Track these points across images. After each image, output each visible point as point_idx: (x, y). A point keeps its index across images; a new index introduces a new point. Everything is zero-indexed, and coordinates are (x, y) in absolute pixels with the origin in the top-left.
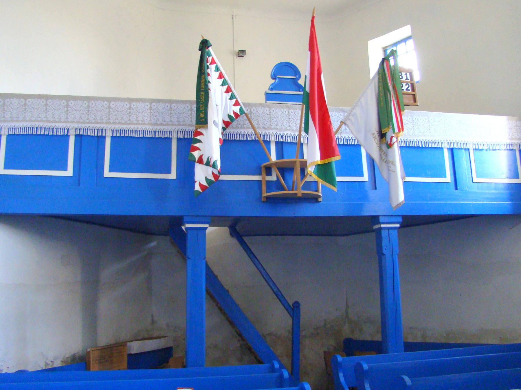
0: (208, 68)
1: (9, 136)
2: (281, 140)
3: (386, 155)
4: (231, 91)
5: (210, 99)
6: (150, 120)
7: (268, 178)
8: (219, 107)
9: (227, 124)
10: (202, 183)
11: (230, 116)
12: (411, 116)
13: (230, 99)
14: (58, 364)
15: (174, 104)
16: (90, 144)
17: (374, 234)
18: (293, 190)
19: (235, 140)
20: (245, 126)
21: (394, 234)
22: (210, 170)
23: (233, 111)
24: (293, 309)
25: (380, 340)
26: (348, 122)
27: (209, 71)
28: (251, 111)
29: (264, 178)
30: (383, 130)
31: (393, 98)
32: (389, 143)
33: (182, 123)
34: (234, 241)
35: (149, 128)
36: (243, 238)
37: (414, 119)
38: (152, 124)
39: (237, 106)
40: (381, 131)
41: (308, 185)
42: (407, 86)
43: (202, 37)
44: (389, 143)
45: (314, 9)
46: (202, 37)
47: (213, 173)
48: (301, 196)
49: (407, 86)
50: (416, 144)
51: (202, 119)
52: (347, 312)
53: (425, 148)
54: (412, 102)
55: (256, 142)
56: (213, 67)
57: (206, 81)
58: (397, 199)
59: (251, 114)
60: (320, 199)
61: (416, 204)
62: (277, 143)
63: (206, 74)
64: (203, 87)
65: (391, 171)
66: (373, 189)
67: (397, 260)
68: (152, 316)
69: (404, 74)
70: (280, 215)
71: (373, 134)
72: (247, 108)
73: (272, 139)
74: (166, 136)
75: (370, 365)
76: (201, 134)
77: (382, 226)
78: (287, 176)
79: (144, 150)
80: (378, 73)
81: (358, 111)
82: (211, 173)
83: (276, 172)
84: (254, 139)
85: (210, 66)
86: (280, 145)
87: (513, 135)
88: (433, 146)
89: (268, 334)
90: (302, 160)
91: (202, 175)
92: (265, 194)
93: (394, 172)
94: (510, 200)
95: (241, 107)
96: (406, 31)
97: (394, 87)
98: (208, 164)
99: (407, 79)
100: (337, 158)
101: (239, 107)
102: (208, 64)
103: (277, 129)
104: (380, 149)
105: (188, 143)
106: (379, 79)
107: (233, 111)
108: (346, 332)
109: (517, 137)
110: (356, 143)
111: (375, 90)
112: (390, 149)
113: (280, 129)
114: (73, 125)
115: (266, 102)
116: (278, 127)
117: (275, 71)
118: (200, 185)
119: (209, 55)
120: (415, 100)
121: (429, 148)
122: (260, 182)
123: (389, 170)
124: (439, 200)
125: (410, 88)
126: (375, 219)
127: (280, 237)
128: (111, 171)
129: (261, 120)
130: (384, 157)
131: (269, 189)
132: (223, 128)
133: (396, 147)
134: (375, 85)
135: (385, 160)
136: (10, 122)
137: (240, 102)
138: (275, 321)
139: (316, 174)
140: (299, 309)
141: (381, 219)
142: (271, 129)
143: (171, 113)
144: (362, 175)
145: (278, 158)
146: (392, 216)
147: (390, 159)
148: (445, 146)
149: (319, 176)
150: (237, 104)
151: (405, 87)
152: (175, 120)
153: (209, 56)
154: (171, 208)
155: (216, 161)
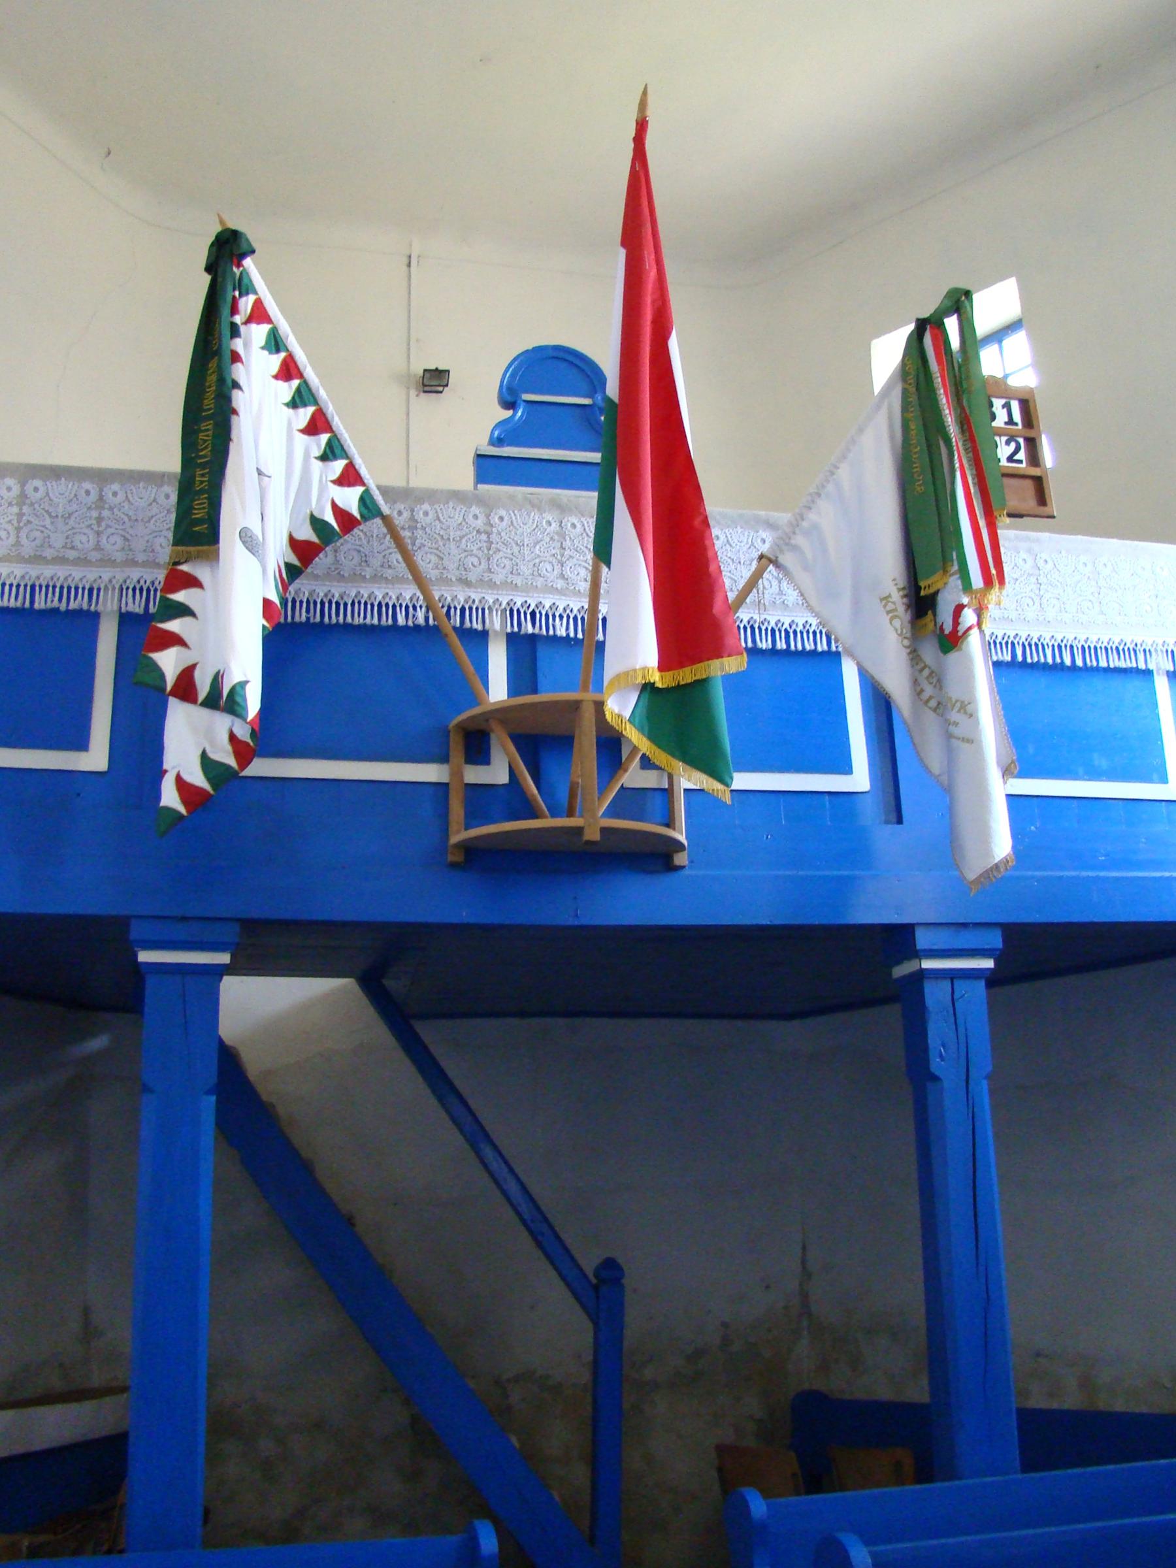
0: (235, 331)
2: (530, 630)
3: (937, 679)
4: (328, 428)
5: (232, 446)
6: (18, 543)
7: (475, 775)
8: (274, 479)
9: (304, 552)
10: (187, 778)
11: (317, 523)
12: (1029, 551)
13: (324, 458)
15: (116, 487)
17: (892, 1014)
18: (570, 813)
19: (347, 627)
20: (389, 573)
22: (222, 723)
23: (334, 506)
24: (596, 1288)
25: (925, 1398)
26: (786, 559)
27: (238, 345)
28: (412, 518)
29: (457, 774)
30: (922, 584)
31: (961, 459)
32: (948, 628)
33: (141, 558)
34: (379, 1033)
36: (413, 1022)
37: (1041, 563)
38: (21, 559)
39: (350, 485)
40: (918, 589)
41: (631, 802)
42: (1013, 445)
43: (222, 222)
44: (948, 628)
45: (645, 93)
46: (222, 222)
47: (233, 738)
48: (596, 836)
49: (1013, 445)
50: (1049, 653)
51: (198, 524)
52: (805, 1297)
53: (1086, 669)
54: (1031, 503)
55: (429, 633)
56: (258, 333)
57: (221, 380)
58: (988, 852)
59: (413, 528)
60: (681, 859)
61: (1061, 878)
62: (515, 641)
63: (227, 357)
64: (209, 402)
65: (957, 739)
66: (887, 822)
67: (985, 1101)
68: (87, 1311)
69: (998, 403)
70: (521, 919)
71: (886, 599)
72: (400, 506)
73: (495, 623)
74: (73, 605)
75: (881, 1548)
76: (193, 582)
77: (927, 964)
78: (551, 765)
80: (904, 371)
81: (825, 515)
82: (225, 738)
83: (504, 746)
84: (421, 620)
85: (243, 329)
86: (525, 649)
88: (1115, 662)
89: (517, 1379)
91: (190, 743)
92: (458, 836)
93: (970, 741)
95: (367, 492)
97: (965, 423)
98: (213, 702)
99: (1011, 421)
100: (733, 664)
101: (358, 490)
102: (238, 319)
103: (516, 587)
104: (914, 656)
106: (905, 392)
107: (334, 506)
108: (804, 1368)
110: (822, 646)
111: (892, 437)
112: (953, 656)
113: (529, 588)
115: (475, 488)
116: (519, 581)
117: (513, 376)
118: (180, 783)
119: (244, 286)
120: (1042, 498)
121: (1098, 669)
122: (442, 788)
123: (949, 736)
124: (1140, 865)
125: (1021, 455)
126: (898, 939)
127: (561, 1021)
129: (454, 551)
130: (929, 690)
131: (474, 816)
132: (288, 566)
133: (974, 642)
134: (890, 419)
135: (933, 703)
137: (364, 472)
138: (546, 1332)
139: (641, 729)
140: (622, 1287)
141: (923, 940)
142: (492, 585)
143: (100, 520)
144: (844, 766)
145: (513, 690)
146: (964, 925)
147: (953, 691)
149: (653, 738)
151: (1004, 451)
152: (113, 545)
153: (245, 292)
154: (79, 887)
155: (243, 684)
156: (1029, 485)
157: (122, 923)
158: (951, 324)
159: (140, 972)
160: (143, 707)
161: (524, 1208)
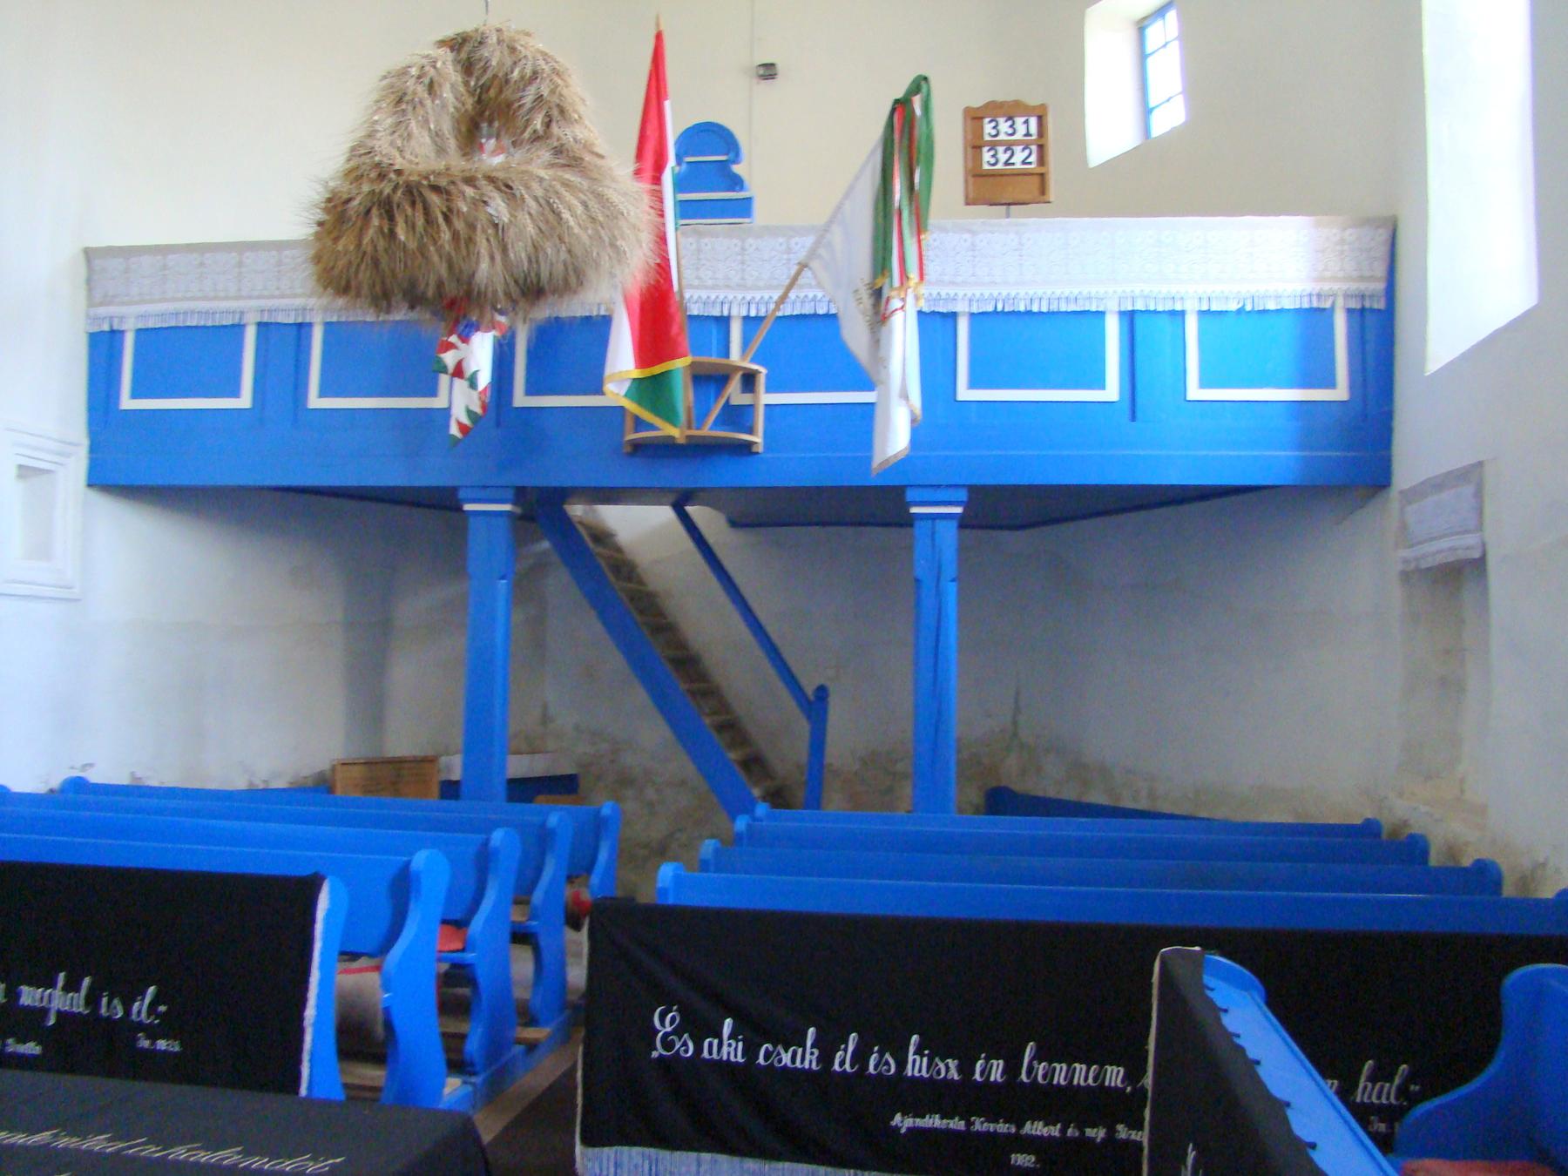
1: (139, 331)
14: (280, 784)
21: (948, 535)
42: (1027, 152)
45: (659, 37)
49: (1027, 152)
52: (1015, 723)
68: (545, 707)
87: (1326, 269)
90: (724, 361)
94: (1301, 447)
99: (1028, 134)
109: (1341, 274)
114: (253, 303)
120: (1043, 190)
125: (1033, 159)
128: (323, 394)
136: (136, 303)
156: (1036, 180)
157: (454, 490)
158: (917, 102)
159: (515, 503)
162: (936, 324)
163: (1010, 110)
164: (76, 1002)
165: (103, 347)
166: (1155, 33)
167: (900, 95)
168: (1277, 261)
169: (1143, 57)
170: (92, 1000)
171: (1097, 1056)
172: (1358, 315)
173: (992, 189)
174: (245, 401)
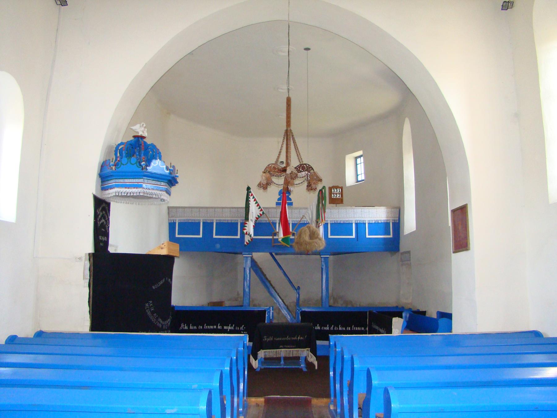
8: (254, 212)
16: (208, 226)
35: (229, 219)
51: (247, 219)
79: (228, 227)
91: (247, 239)
96: (360, 153)
105: (243, 225)
119: (250, 192)
148: (354, 222)
150: (261, 210)
152: (239, 215)
158: (323, 190)
160: (243, 235)
161: (269, 285)
162: (326, 225)
163: (336, 187)
164: (232, 328)
165: (172, 226)
166: (358, 160)
167: (285, 129)
168: (379, 214)
169: (356, 164)
170: (235, 327)
171: (361, 327)
172: (394, 224)
173: (334, 201)
174: (201, 236)
